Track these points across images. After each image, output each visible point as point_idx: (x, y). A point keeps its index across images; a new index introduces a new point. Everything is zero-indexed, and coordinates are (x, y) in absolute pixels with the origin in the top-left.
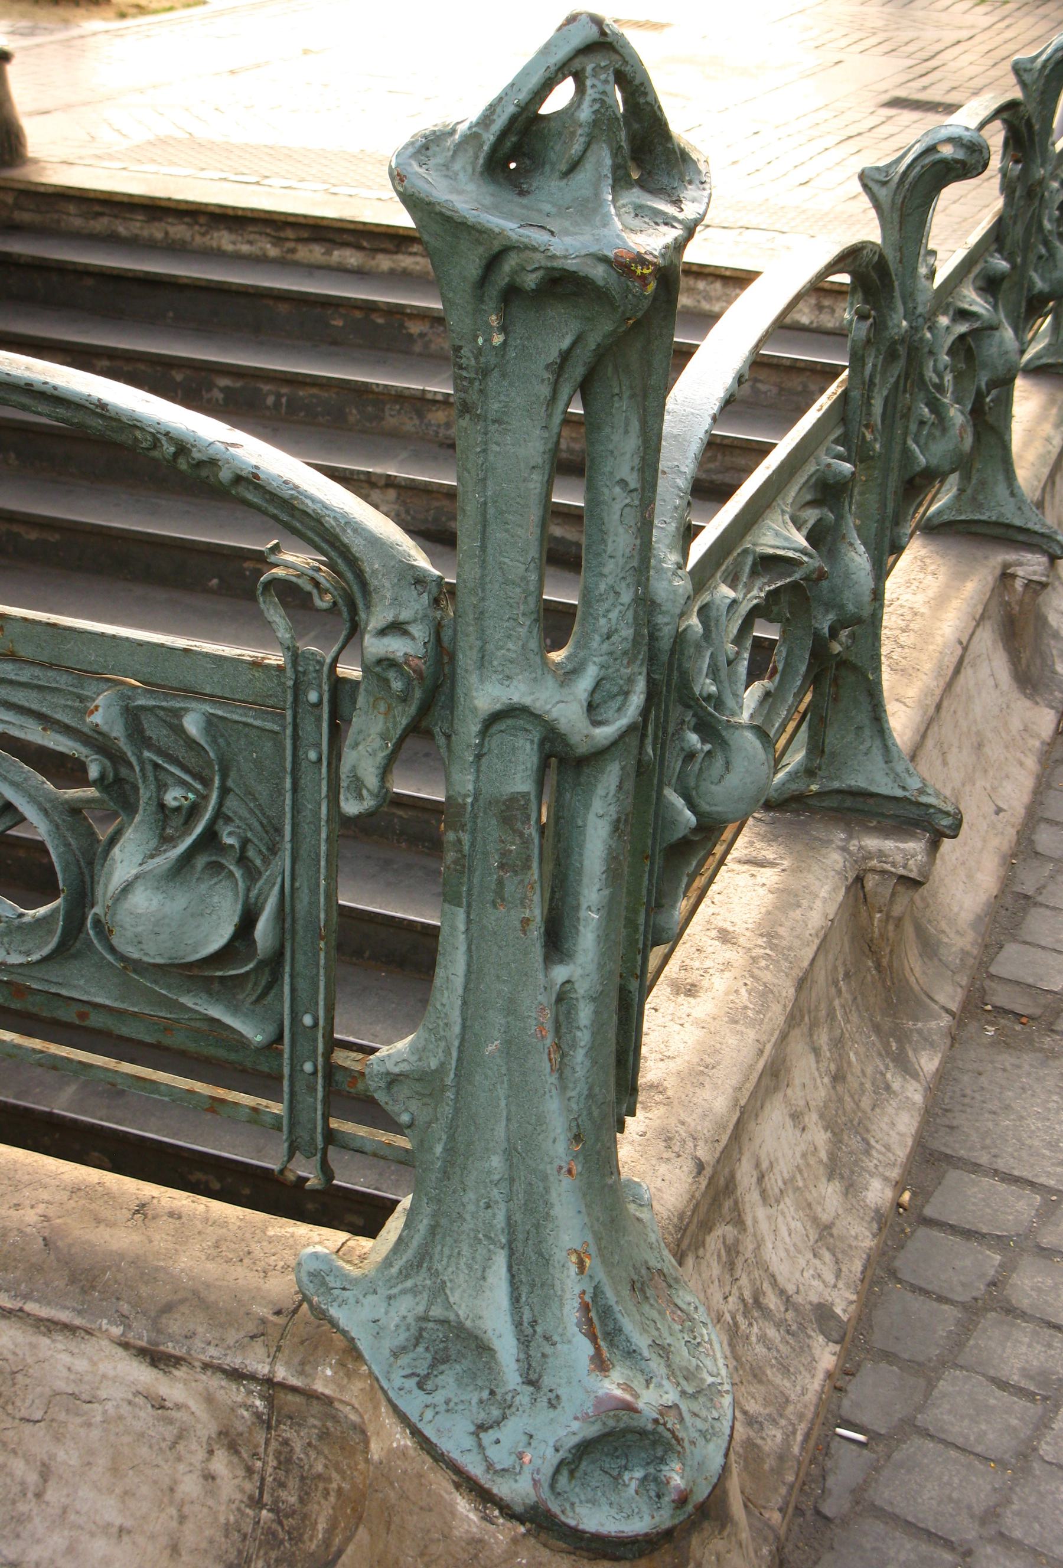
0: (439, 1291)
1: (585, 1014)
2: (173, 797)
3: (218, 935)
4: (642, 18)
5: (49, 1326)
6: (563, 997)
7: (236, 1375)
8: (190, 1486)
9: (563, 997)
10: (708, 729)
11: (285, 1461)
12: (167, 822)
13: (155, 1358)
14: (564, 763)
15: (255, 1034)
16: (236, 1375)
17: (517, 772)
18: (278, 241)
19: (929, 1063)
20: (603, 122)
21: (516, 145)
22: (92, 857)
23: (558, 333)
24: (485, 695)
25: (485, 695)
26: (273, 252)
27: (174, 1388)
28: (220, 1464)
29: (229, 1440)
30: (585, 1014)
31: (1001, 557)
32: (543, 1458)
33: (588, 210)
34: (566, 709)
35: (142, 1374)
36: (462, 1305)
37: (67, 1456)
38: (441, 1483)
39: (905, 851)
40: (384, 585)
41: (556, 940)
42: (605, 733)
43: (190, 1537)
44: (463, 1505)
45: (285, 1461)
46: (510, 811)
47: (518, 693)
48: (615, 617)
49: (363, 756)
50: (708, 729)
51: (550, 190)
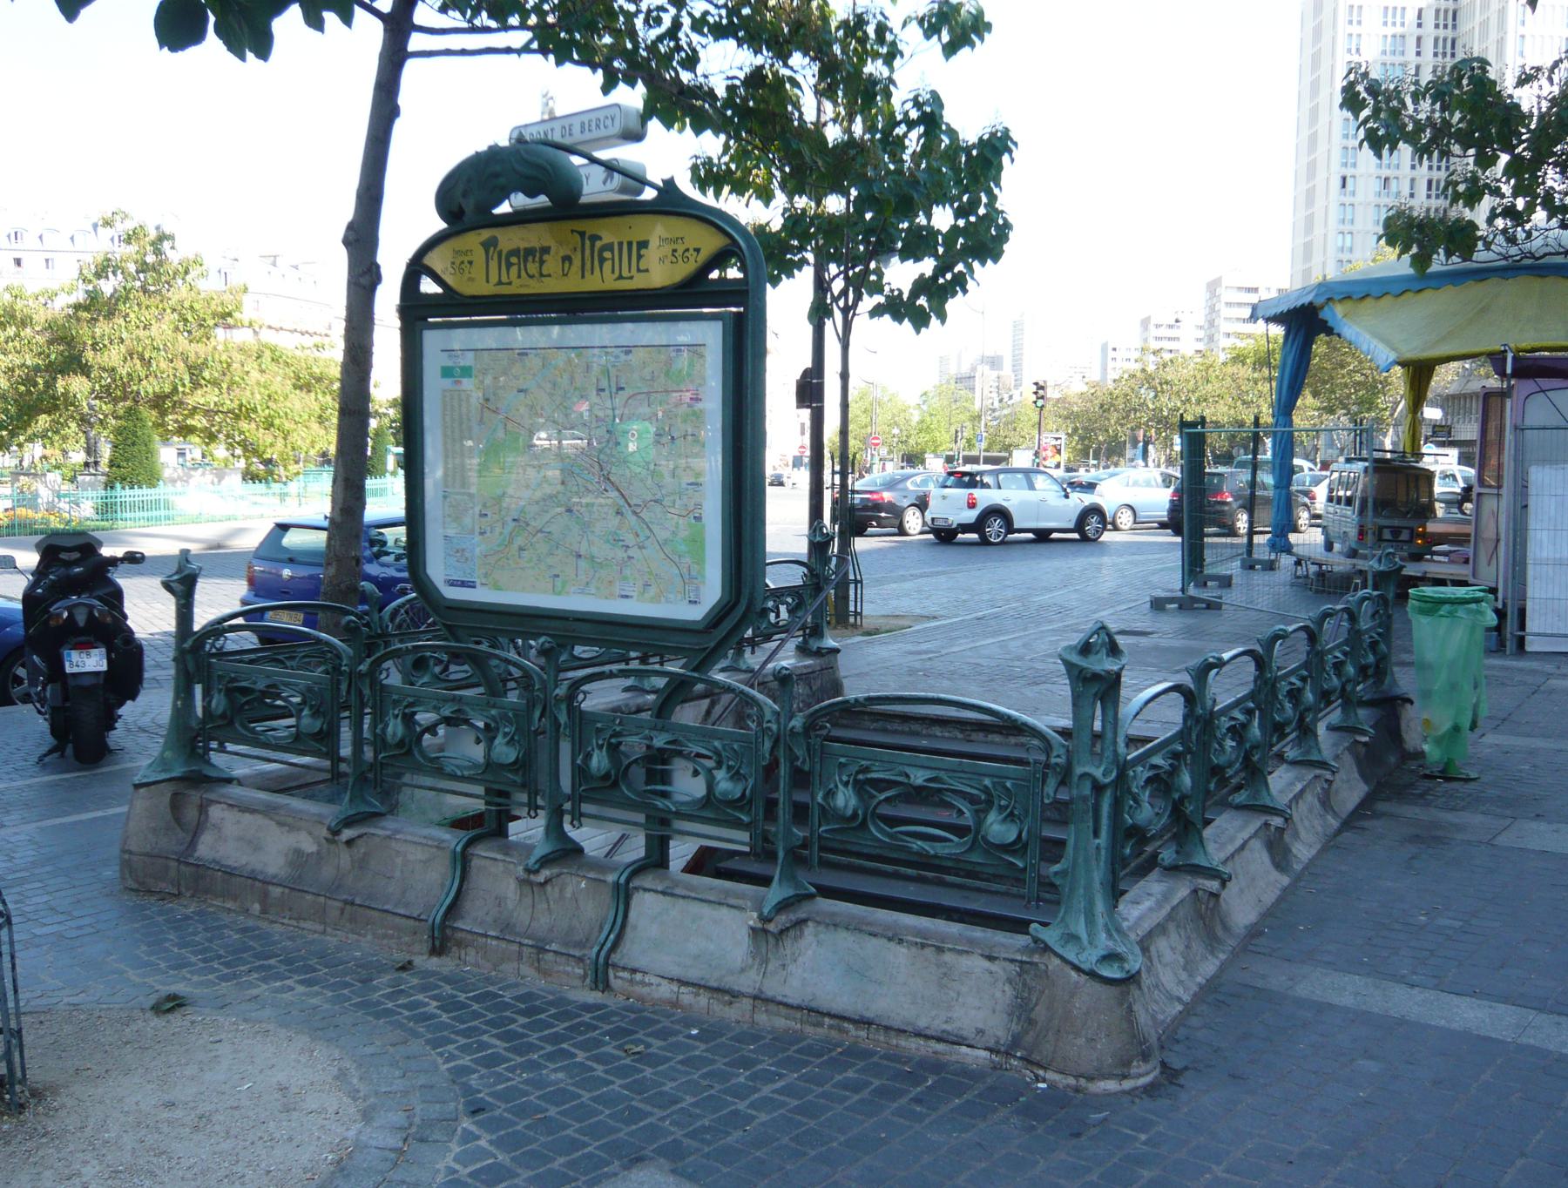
0: (1067, 926)
1: (1103, 852)
2: (1003, 803)
3: (1012, 837)
4: (338, 262)
5: (961, 952)
6: (1098, 848)
7: (1012, 961)
8: (998, 994)
9: (1098, 848)
10: (1136, 801)
11: (1025, 984)
12: (1002, 809)
13: (991, 958)
14: (1098, 788)
15: (1021, 864)
16: (1012, 961)
17: (1087, 789)
18: (962, 731)
19: (1222, 956)
20: (1103, 644)
21: (1086, 649)
22: (980, 822)
23: (1095, 688)
24: (1079, 770)
25: (1079, 770)
26: (960, 736)
27: (994, 967)
28: (1007, 988)
29: (1010, 981)
30: (1103, 852)
31: (1264, 818)
32: (1094, 959)
33: (1100, 661)
34: (1098, 773)
35: (987, 964)
36: (1073, 930)
37: (964, 989)
38: (1068, 969)
39: (1214, 885)
40: (1055, 746)
41: (1096, 834)
42: (1107, 780)
43: (998, 1008)
44: (1073, 974)
45: (1025, 984)
46: (1085, 799)
47: (1088, 769)
48: (1108, 754)
49: (1050, 789)
50: (1136, 801)
51: (1092, 658)
